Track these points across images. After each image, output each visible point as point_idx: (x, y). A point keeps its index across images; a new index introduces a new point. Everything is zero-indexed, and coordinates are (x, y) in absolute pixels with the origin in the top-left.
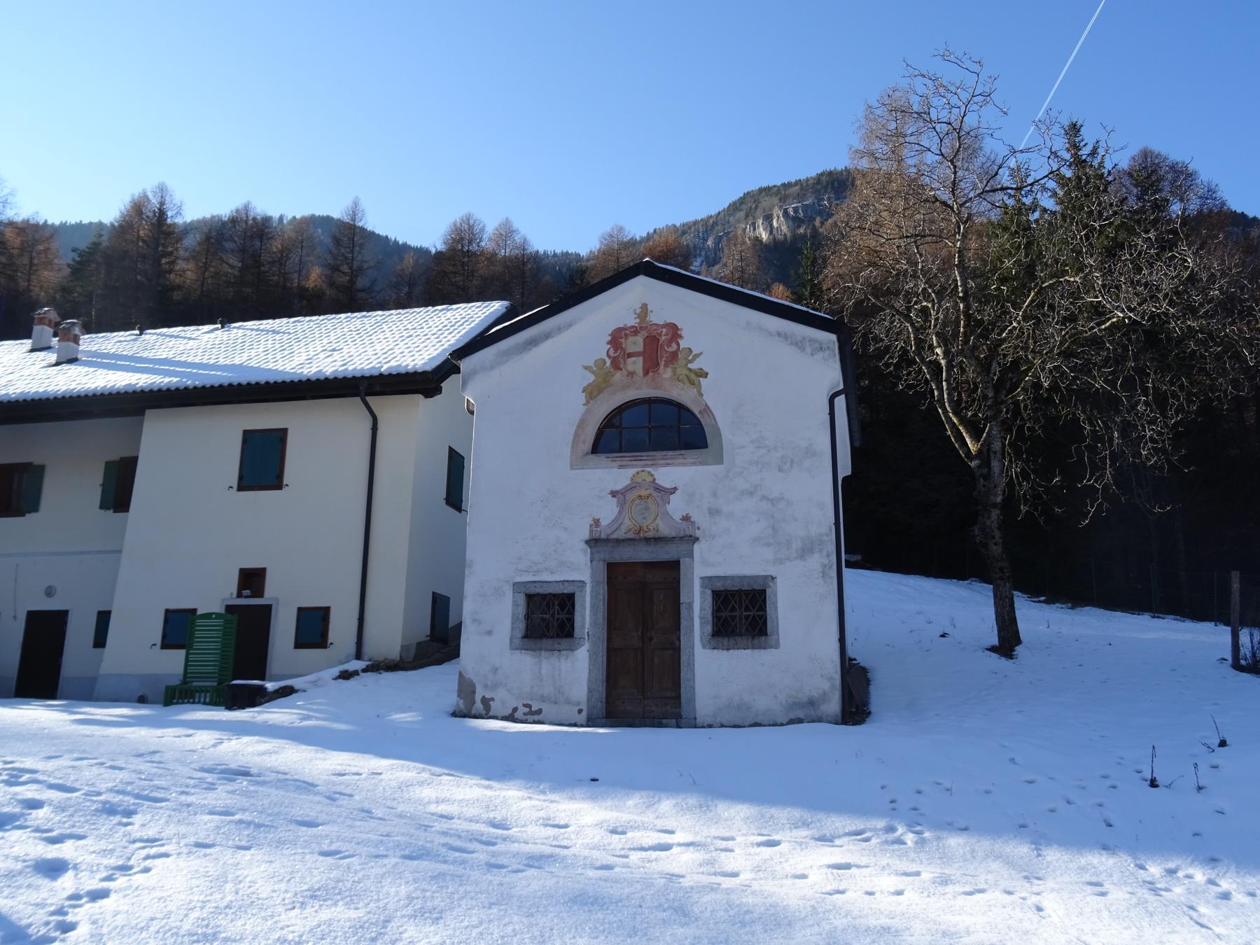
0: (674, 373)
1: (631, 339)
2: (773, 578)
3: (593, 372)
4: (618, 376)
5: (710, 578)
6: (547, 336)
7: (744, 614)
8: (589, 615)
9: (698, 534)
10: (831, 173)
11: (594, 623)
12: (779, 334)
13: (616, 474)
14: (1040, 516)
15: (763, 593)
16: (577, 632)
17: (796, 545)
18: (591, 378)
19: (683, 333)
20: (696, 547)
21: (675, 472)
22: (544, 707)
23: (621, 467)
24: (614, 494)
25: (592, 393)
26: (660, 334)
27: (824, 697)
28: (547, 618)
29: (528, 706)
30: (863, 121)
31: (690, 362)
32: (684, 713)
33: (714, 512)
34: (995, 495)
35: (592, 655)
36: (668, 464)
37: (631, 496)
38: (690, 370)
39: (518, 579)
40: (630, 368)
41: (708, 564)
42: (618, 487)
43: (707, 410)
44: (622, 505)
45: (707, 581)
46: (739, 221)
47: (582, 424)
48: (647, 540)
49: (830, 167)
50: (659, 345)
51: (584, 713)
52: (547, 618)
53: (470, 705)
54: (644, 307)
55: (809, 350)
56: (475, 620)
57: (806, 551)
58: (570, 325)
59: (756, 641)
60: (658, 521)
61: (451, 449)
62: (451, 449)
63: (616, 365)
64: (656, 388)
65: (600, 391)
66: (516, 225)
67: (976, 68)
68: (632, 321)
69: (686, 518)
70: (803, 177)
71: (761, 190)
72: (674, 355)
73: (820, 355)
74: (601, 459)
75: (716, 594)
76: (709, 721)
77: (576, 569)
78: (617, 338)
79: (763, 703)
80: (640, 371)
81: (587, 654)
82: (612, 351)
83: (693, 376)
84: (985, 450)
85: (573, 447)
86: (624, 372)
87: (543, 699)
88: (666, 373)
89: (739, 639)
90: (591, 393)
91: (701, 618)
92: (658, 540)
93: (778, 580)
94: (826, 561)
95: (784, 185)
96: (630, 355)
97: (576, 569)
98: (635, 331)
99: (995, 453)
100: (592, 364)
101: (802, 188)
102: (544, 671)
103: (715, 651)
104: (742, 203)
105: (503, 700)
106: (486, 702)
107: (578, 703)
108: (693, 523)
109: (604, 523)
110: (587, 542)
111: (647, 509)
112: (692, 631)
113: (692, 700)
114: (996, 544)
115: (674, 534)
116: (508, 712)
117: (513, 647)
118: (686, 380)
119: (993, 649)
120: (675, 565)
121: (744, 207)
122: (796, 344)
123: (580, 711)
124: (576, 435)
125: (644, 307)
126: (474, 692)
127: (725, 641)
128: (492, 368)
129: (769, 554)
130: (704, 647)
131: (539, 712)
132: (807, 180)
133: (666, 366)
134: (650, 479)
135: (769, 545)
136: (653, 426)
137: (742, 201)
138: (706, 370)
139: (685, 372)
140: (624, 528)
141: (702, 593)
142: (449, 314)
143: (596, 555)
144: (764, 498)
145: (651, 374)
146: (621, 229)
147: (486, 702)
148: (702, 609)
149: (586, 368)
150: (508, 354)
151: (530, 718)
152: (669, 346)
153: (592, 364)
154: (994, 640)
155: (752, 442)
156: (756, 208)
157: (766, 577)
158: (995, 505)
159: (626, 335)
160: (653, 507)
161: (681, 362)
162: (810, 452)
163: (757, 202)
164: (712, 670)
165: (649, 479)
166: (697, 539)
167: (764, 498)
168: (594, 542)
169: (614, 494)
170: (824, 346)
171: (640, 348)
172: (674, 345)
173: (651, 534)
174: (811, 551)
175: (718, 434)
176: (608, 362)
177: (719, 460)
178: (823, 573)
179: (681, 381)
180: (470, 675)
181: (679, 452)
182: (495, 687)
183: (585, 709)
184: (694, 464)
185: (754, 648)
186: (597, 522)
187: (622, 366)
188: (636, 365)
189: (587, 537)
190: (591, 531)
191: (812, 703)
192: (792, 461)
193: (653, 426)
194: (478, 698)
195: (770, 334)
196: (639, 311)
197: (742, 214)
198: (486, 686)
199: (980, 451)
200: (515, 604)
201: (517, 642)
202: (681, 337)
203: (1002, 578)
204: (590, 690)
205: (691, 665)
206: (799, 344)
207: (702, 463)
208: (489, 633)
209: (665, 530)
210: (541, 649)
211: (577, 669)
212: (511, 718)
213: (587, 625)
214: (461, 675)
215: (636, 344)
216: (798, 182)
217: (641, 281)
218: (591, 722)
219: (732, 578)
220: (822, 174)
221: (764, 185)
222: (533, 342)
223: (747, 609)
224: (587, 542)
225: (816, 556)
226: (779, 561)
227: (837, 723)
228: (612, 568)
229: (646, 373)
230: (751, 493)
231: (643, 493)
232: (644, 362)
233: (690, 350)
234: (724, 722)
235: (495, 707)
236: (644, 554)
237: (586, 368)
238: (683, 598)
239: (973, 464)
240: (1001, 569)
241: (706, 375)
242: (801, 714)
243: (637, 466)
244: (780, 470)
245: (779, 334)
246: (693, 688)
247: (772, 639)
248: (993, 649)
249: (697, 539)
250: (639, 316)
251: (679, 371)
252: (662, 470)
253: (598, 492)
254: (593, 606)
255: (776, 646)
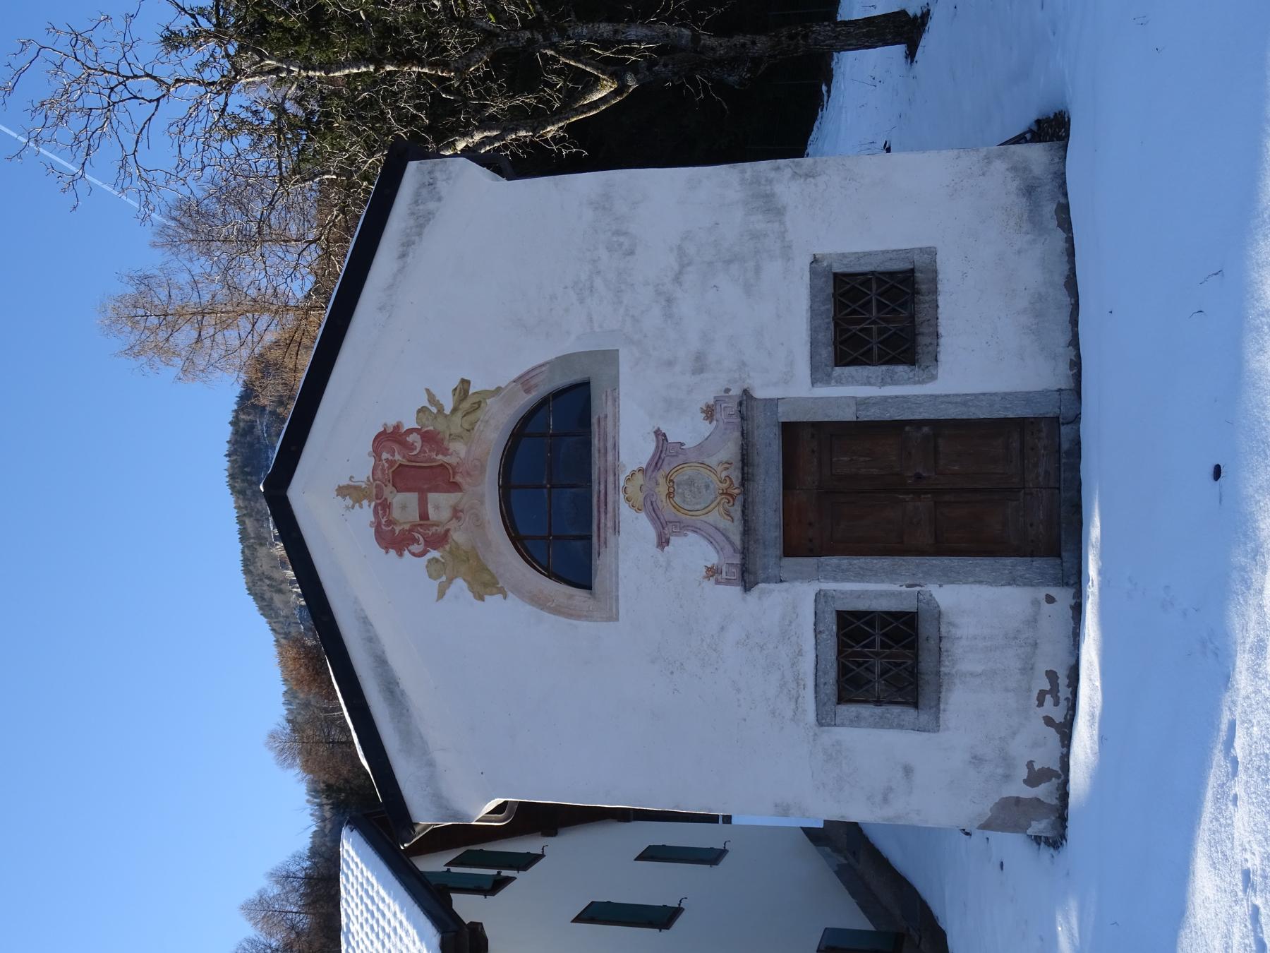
0: (460, 437)
1: (396, 514)
2: (815, 260)
3: (450, 581)
4: (458, 537)
5: (814, 369)
6: (381, 662)
7: (876, 311)
8: (876, 586)
9: (736, 391)
10: (232, 476)
11: (891, 575)
12: (403, 256)
13: (629, 542)
14: (711, 12)
15: (839, 278)
16: (907, 606)
17: (759, 222)
18: (460, 584)
19: (392, 422)
20: (759, 394)
21: (630, 434)
22: (1042, 666)
23: (616, 530)
24: (663, 542)
25: (485, 583)
26: (391, 463)
27: (1018, 169)
28: (881, 664)
29: (1042, 694)
30: (143, 359)
31: (441, 409)
32: (1049, 410)
33: (700, 365)
34: (681, 36)
35: (948, 578)
36: (615, 446)
37: (667, 511)
38: (455, 410)
39: (811, 716)
40: (446, 514)
41: (789, 370)
42: (651, 533)
43: (525, 381)
44: (682, 528)
45: (818, 375)
46: (287, 603)
47: (539, 602)
48: (746, 479)
49: (223, 478)
50: (411, 464)
51: (1053, 591)
52: (881, 664)
53: (1045, 815)
54: (343, 491)
55: (432, 205)
56: (885, 800)
57: (770, 207)
58: (365, 621)
59: (923, 287)
60: (713, 461)
61: (578, 919)
62: (578, 919)
63: (438, 540)
64: (483, 469)
65: (484, 568)
66: (252, 894)
67: (32, 49)
68: (366, 513)
69: (709, 413)
70: (234, 513)
71: (247, 571)
72: (430, 438)
73: (442, 186)
74: (601, 566)
75: (842, 359)
76: (1064, 368)
77: (795, 609)
78: (393, 539)
79: (1032, 268)
80: (452, 498)
81: (947, 588)
82: (416, 548)
83: (466, 405)
84: (610, 69)
85: (579, 617)
86: (453, 524)
87: (1028, 669)
88: (458, 451)
89: (919, 318)
90: (485, 585)
91: (883, 383)
92: (746, 460)
93: (819, 251)
94: (788, 173)
95: (242, 540)
96: (424, 516)
97: (795, 609)
98: (383, 507)
99: (616, 32)
100: (436, 584)
101: (250, 516)
102: (979, 668)
103: (941, 357)
104: (263, 599)
105: (1034, 745)
106: (1034, 778)
107: (1035, 602)
108: (717, 400)
109: (713, 558)
110: (747, 586)
111: (691, 482)
112: (905, 399)
113: (1028, 397)
114: (754, 43)
115: (737, 434)
116: (1053, 736)
117: (934, 726)
118: (471, 417)
119: (911, 55)
120: (790, 431)
121: (267, 595)
122: (421, 226)
123: (1050, 599)
124: (557, 611)
125: (343, 491)
126: (1018, 801)
127: (923, 340)
128: (431, 764)
129: (773, 269)
130: (933, 378)
131: (1052, 675)
132: (238, 508)
133: (445, 452)
134: (639, 476)
135: (758, 270)
136: (546, 482)
137: (259, 597)
138: (455, 383)
139: (457, 418)
140: (724, 523)
141: (840, 382)
142: (355, 928)
143: (772, 572)
144: (677, 279)
145: (458, 479)
146: (273, 736)
147: (1034, 778)
148: (868, 383)
149: (441, 594)
150: (407, 734)
151: (1064, 692)
152: (411, 447)
153: (436, 584)
154: (899, 50)
155: (582, 301)
156: (269, 578)
157: (813, 273)
158: (696, 38)
159: (389, 523)
160: (688, 472)
161: (440, 426)
162: (603, 204)
163: (263, 577)
164: (977, 361)
165: (639, 479)
166: (745, 392)
167: (677, 279)
168: (747, 578)
169: (663, 542)
170: (427, 179)
171: (412, 498)
172: (411, 438)
173: (736, 475)
174: (769, 197)
175: (565, 361)
176: (434, 554)
177: (610, 357)
178: (807, 176)
179: (473, 424)
180: (985, 808)
181: (595, 427)
182: (1006, 760)
183: (1042, 592)
184: (615, 400)
185: (934, 291)
186: (712, 572)
187: (441, 530)
188: (440, 504)
189: (736, 590)
190: (728, 582)
191: (1029, 191)
192: (617, 233)
193: (546, 482)
194: (1027, 793)
195: (401, 270)
196: (349, 501)
197: (277, 598)
198: (1007, 777)
199: (613, 76)
200: (856, 722)
201: (924, 718)
202: (397, 427)
203: (805, 37)
204: (1012, 582)
205: (965, 400)
206: (422, 221)
207: (615, 388)
208: (908, 771)
209: (729, 450)
210: (938, 673)
211: (974, 607)
212: (1065, 731)
213: (894, 588)
214: (986, 826)
215: (405, 505)
216: (241, 521)
217: (300, 494)
218: (1074, 579)
219: (814, 331)
220: (232, 487)
221: (240, 566)
222: (391, 688)
223: (866, 306)
224: (747, 586)
225: (779, 189)
226: (786, 251)
227: (1065, 148)
228: (790, 550)
229: (455, 487)
230: (669, 301)
231: (663, 489)
232: (436, 489)
233: (422, 410)
234: (1068, 337)
235: (1046, 758)
236: (769, 485)
237: (441, 594)
238: (848, 415)
239: (633, 84)
240: (792, 37)
241: (465, 383)
242: (1049, 209)
243: (616, 503)
244: (632, 253)
245: (403, 256)
246: (1005, 396)
247: (920, 261)
248: (911, 55)
249: (745, 392)
250: (358, 501)
251: (456, 429)
252: (624, 457)
253: (656, 567)
254: (861, 576)
255: (932, 252)
